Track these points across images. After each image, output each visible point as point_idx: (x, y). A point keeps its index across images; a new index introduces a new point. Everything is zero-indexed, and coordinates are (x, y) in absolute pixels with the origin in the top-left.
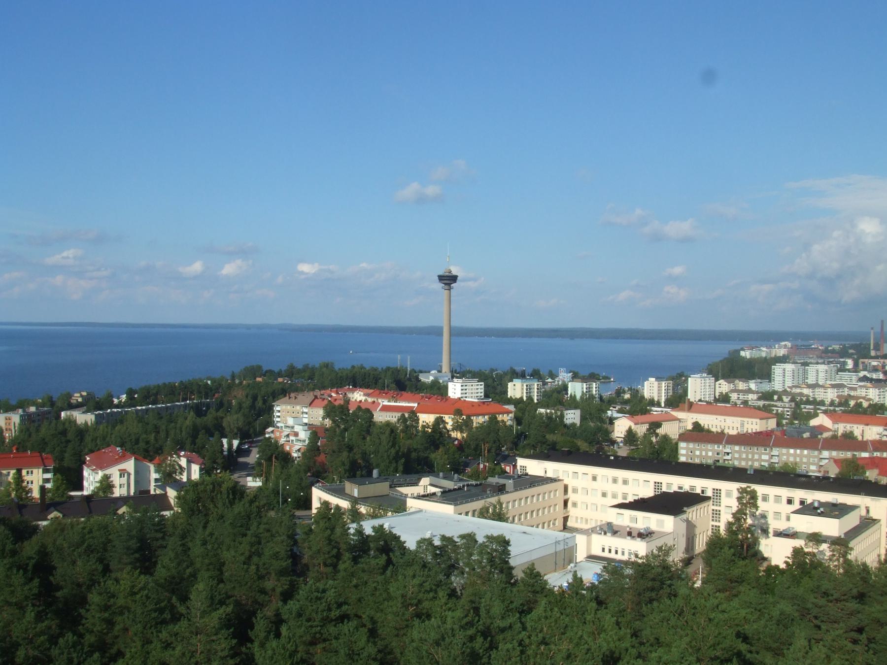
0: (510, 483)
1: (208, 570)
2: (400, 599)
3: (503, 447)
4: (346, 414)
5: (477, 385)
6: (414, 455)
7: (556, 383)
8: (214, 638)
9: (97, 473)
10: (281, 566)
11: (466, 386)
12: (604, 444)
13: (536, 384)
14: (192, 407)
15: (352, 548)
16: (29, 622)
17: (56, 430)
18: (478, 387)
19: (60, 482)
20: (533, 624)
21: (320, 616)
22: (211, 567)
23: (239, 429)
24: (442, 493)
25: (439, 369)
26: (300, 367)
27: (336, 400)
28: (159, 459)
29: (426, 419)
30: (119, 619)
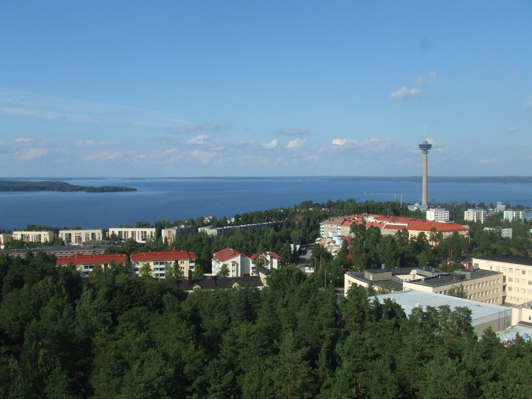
0: (468, 274)
1: (288, 323)
2: (411, 347)
3: (462, 251)
4: (364, 230)
5: (445, 213)
6: (406, 255)
7: (495, 211)
8: (299, 365)
9: (220, 263)
10: (329, 321)
11: (438, 213)
12: (528, 250)
13: (482, 212)
14: (272, 226)
15: (371, 312)
16: (191, 350)
17: (196, 238)
18: (445, 214)
19: (199, 268)
20: (511, 370)
21: (361, 355)
22: (290, 321)
23: (300, 239)
24: (425, 279)
25: (420, 203)
26: (335, 201)
27: (357, 221)
28: (255, 256)
29: (414, 233)
30: (240, 350)
